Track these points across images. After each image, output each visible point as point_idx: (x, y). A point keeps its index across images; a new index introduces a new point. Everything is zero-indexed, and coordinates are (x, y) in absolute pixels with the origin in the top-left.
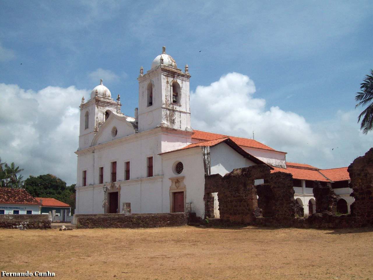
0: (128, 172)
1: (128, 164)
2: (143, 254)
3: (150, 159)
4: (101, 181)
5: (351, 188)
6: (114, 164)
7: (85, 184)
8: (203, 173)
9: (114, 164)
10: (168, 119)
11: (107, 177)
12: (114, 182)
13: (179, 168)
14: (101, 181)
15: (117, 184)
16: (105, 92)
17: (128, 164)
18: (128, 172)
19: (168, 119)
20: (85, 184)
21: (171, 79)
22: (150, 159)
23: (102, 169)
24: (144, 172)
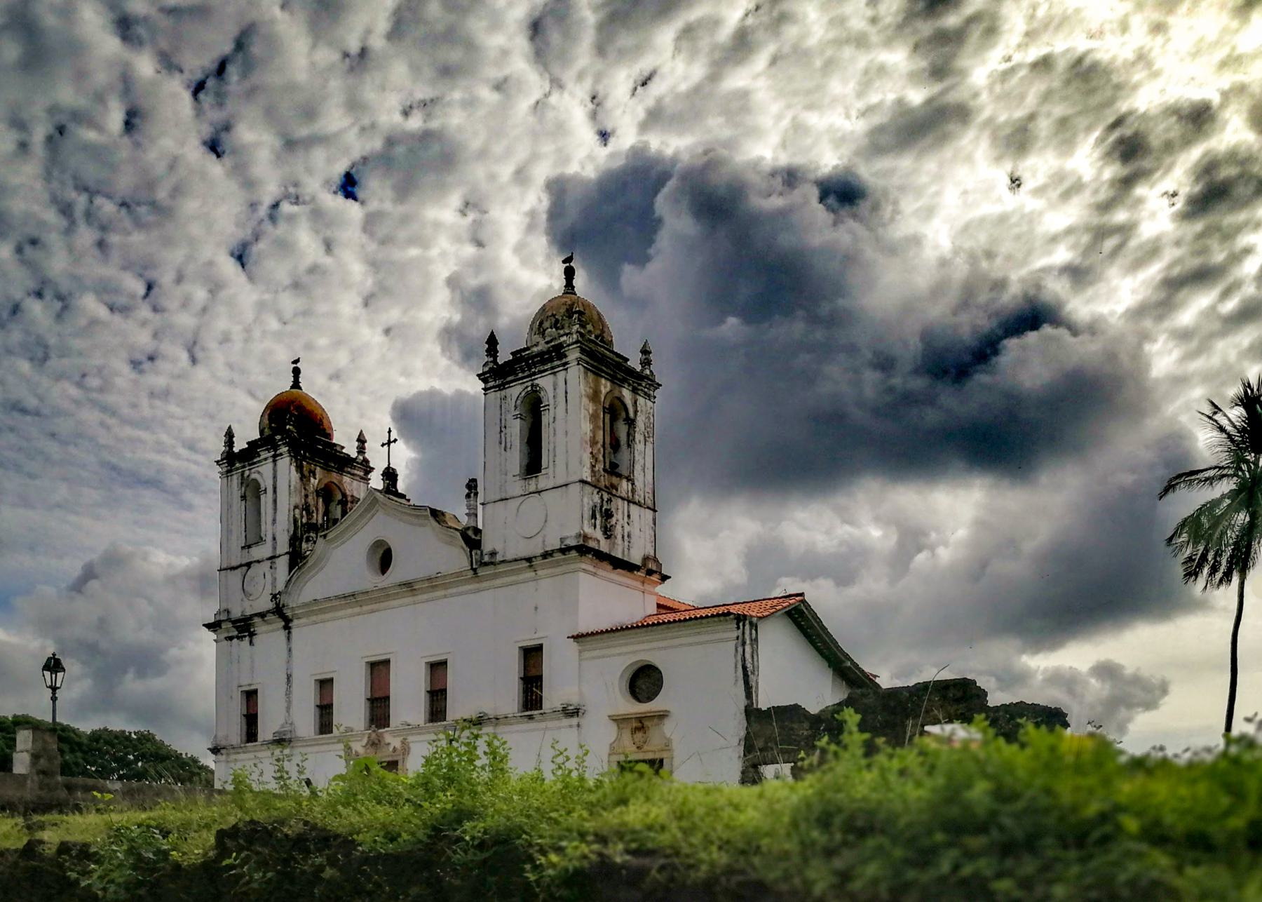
0: (437, 701)
1: (437, 668)
2: (270, 190)
3: (532, 655)
4: (325, 726)
5: (894, 692)
6: (379, 669)
7: (251, 734)
8: (742, 702)
9: (379, 669)
10: (598, 522)
11: (351, 709)
12: (379, 727)
13: (644, 681)
14: (325, 726)
15: (392, 740)
16: (212, 106)
17: (437, 668)
18: (437, 701)
19: (598, 522)
20: (251, 734)
21: (605, 386)
22: (532, 655)
23: (325, 685)
24: (508, 698)
